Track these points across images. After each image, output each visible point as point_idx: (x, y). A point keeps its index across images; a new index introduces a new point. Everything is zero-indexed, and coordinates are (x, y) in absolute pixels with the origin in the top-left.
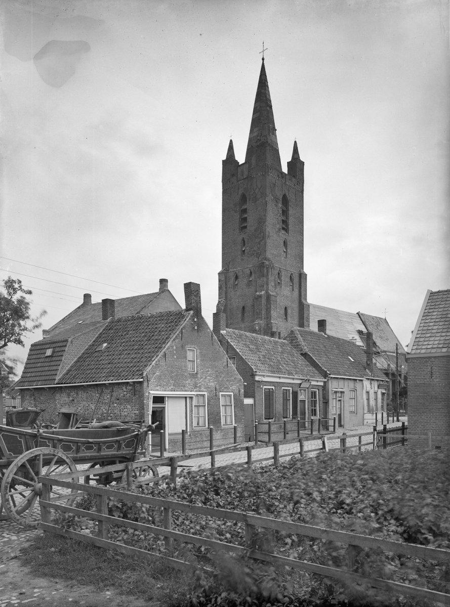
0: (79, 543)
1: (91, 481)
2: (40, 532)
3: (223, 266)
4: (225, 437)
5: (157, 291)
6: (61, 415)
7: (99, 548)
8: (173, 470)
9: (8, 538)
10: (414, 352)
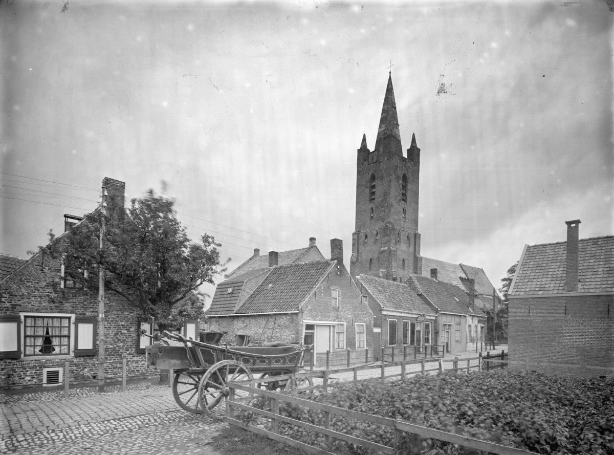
0: (256, 435)
1: (262, 387)
2: (226, 425)
3: (356, 229)
4: (358, 357)
5: (308, 246)
6: (237, 336)
7: (272, 440)
8: (326, 381)
9: (202, 428)
10: (514, 294)
